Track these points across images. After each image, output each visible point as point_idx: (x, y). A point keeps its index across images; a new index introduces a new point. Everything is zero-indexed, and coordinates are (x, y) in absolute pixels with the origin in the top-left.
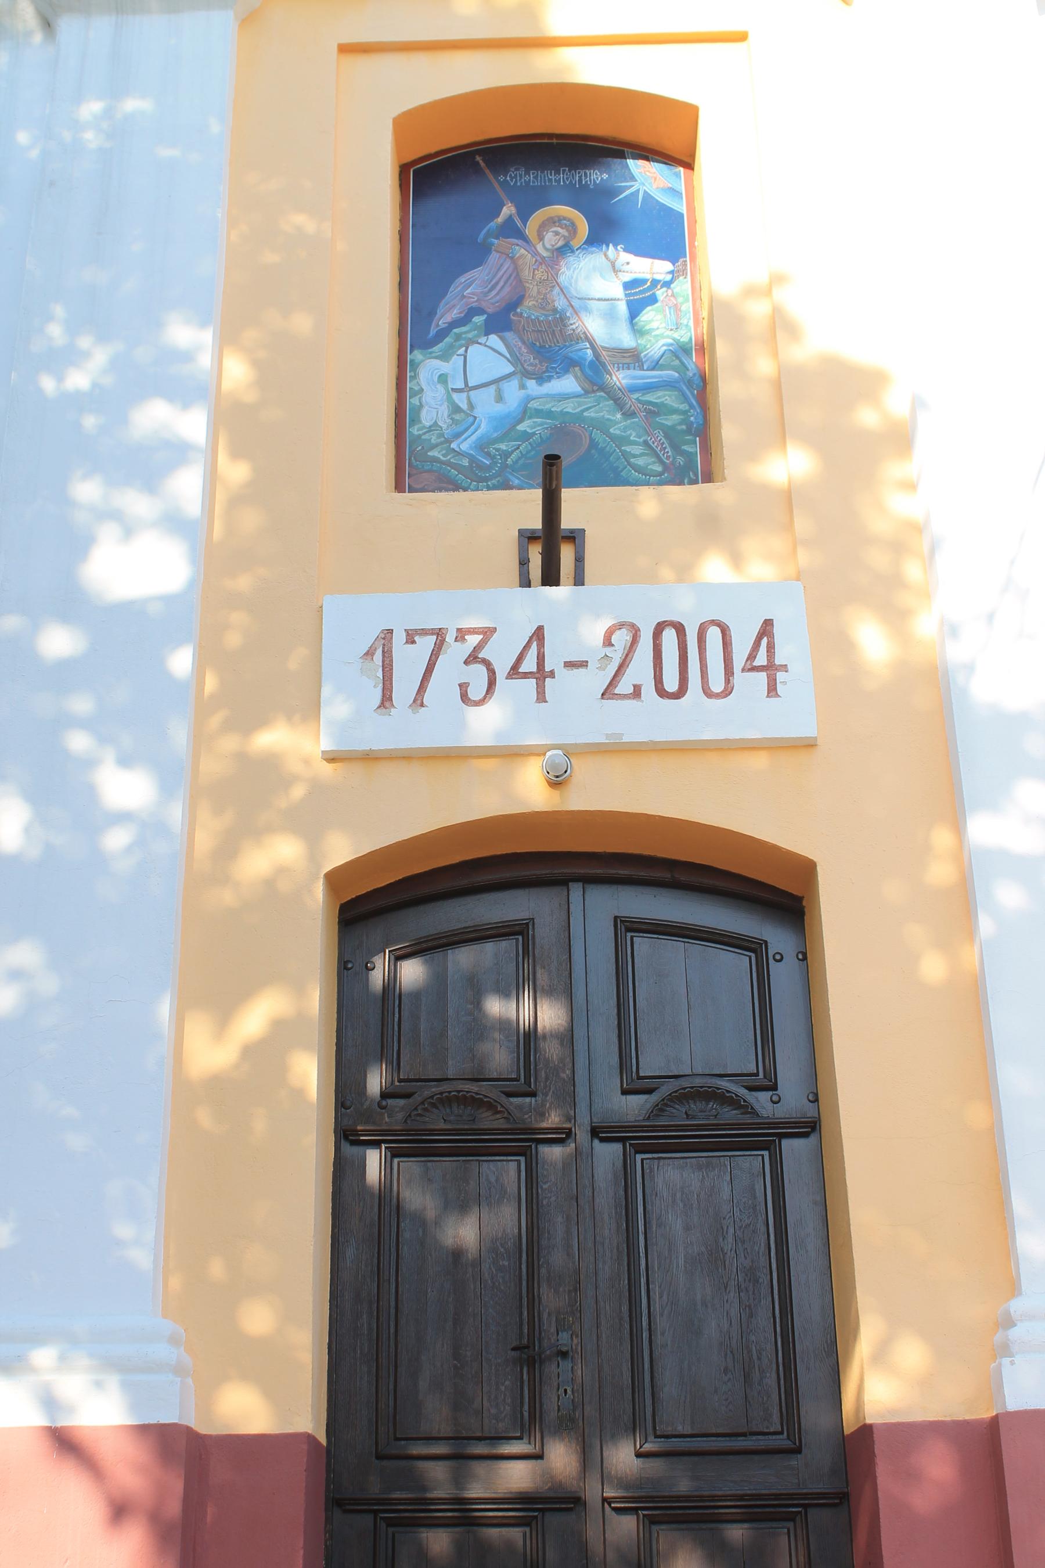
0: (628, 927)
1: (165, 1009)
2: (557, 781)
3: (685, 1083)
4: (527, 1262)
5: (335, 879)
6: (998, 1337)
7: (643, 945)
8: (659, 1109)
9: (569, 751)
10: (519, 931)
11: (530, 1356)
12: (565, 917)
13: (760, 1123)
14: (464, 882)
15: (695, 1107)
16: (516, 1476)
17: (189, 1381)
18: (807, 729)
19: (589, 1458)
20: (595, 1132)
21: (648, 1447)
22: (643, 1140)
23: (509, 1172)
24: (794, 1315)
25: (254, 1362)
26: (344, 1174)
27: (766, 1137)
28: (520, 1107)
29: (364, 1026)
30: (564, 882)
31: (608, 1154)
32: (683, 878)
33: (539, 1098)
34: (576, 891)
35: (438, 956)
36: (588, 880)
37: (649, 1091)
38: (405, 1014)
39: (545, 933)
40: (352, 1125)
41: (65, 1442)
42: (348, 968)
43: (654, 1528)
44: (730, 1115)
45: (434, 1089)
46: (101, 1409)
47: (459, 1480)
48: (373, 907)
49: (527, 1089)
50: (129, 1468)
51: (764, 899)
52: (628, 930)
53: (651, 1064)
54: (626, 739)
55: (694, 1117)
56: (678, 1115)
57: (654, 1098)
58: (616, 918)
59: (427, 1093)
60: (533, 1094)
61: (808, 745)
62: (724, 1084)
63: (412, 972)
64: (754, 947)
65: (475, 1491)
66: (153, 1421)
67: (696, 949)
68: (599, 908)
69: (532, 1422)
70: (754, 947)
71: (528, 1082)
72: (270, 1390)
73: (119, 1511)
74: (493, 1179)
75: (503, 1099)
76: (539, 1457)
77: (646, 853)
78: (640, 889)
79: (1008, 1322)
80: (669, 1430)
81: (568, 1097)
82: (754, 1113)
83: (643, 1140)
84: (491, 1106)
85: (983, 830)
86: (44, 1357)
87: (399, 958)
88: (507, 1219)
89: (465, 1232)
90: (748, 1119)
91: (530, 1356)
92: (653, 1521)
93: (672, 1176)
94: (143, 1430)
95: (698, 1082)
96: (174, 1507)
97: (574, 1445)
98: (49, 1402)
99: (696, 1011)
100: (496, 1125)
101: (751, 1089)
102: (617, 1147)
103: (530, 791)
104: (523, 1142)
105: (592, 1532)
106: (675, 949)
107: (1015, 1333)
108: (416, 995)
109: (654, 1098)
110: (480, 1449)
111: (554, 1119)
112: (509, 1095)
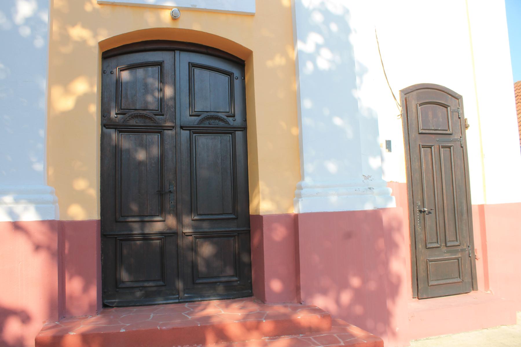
0: (193, 66)
1: (44, 84)
2: (174, 18)
3: (209, 114)
4: (213, 232)
5: (101, 44)
6: (297, 191)
7: (197, 71)
8: (201, 121)
9: (180, 9)
10: (160, 64)
11: (161, 193)
12: (173, 61)
13: (232, 129)
14: (142, 48)
15: (212, 121)
16: (158, 226)
17: (57, 204)
18: (251, 9)
19: (179, 221)
20: (182, 127)
21: (196, 218)
22: (195, 130)
23: (156, 137)
24: (238, 182)
25: (79, 198)
26: (103, 137)
27: (231, 131)
28: (159, 119)
29: (112, 93)
30: (174, 50)
31: (185, 134)
32: (210, 52)
33: (165, 116)
34: (177, 52)
35: (134, 71)
36: (181, 50)
37: (199, 116)
38: (123, 88)
39: (168, 66)
40: (107, 124)
41: (17, 226)
42: (104, 73)
43: (120, 134)
44: (221, 124)
45: (133, 112)
46: (29, 216)
47: (142, 228)
48: (112, 53)
49: (161, 113)
50: (41, 235)
51: (235, 62)
52: (193, 66)
53: (198, 108)
54: (197, 7)
55: (211, 124)
56: (206, 124)
57: (200, 118)
58: (189, 63)
59: (130, 114)
60: (163, 115)
61: (252, 15)
62: (220, 115)
63: (125, 75)
64: (229, 74)
65: (147, 231)
66: (46, 219)
67: (213, 73)
68: (185, 59)
69: (162, 211)
70: (229, 74)
71: (161, 111)
72: (84, 207)
73: (37, 247)
74: (150, 140)
75: (154, 116)
76: (164, 221)
77: (199, 43)
78: (197, 54)
79: (300, 188)
80: (201, 213)
81: (174, 118)
82: (228, 123)
83: (195, 130)
84: (150, 118)
85: (300, 45)
86: (8, 199)
87: (121, 71)
88: (155, 151)
89: (141, 155)
90: (226, 125)
91: (161, 193)
92: (196, 238)
93: (204, 142)
94: (43, 222)
95: (212, 114)
96: (55, 245)
97: (172, 215)
98: (11, 213)
99: (212, 91)
100: (152, 124)
101: (227, 116)
102: (188, 132)
103: (165, 20)
104: (160, 130)
105: (180, 242)
106: (206, 73)
107: (304, 191)
108: (127, 83)
109: (200, 118)
110: (147, 219)
111: (169, 124)
112: (155, 115)
